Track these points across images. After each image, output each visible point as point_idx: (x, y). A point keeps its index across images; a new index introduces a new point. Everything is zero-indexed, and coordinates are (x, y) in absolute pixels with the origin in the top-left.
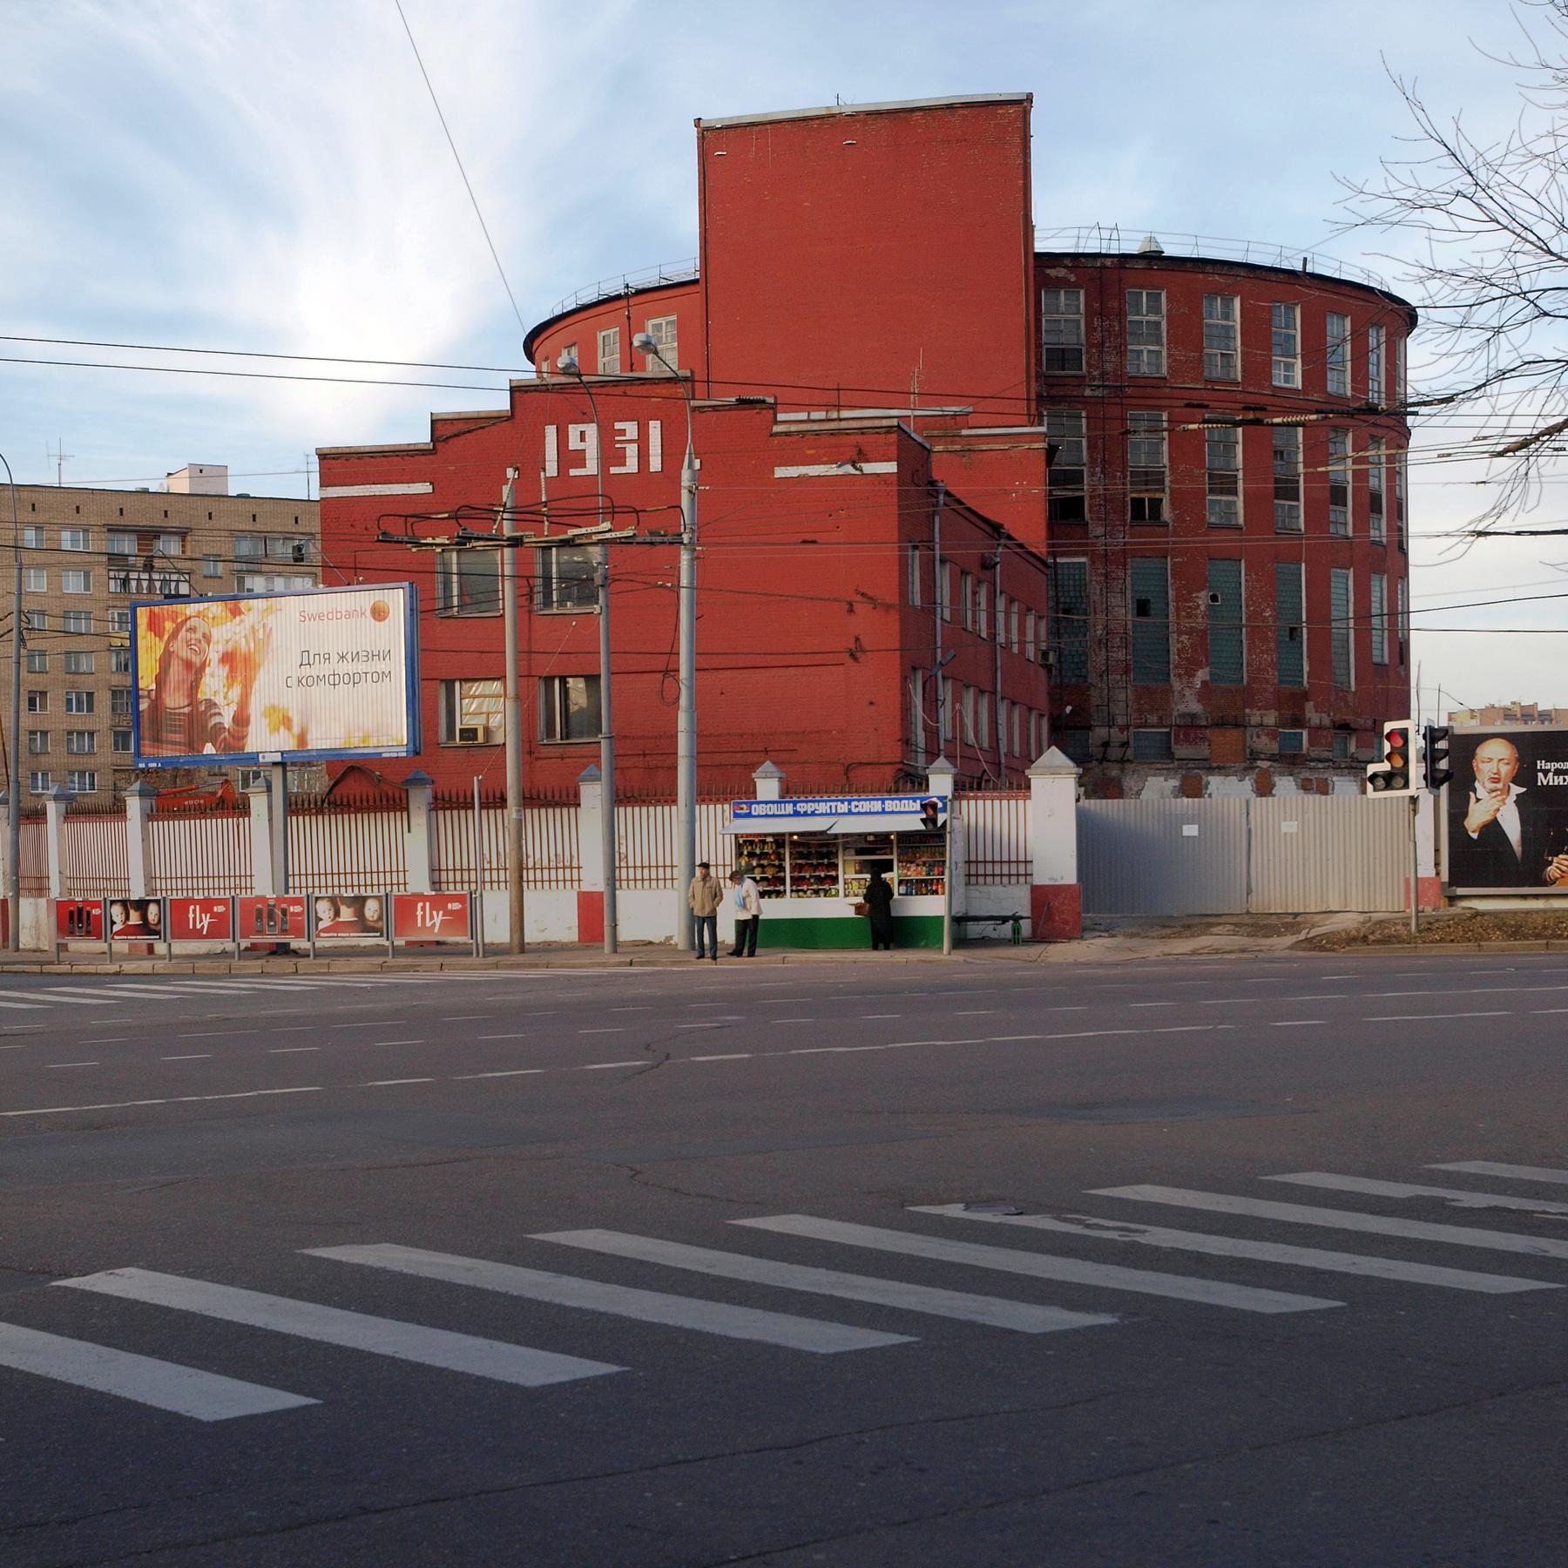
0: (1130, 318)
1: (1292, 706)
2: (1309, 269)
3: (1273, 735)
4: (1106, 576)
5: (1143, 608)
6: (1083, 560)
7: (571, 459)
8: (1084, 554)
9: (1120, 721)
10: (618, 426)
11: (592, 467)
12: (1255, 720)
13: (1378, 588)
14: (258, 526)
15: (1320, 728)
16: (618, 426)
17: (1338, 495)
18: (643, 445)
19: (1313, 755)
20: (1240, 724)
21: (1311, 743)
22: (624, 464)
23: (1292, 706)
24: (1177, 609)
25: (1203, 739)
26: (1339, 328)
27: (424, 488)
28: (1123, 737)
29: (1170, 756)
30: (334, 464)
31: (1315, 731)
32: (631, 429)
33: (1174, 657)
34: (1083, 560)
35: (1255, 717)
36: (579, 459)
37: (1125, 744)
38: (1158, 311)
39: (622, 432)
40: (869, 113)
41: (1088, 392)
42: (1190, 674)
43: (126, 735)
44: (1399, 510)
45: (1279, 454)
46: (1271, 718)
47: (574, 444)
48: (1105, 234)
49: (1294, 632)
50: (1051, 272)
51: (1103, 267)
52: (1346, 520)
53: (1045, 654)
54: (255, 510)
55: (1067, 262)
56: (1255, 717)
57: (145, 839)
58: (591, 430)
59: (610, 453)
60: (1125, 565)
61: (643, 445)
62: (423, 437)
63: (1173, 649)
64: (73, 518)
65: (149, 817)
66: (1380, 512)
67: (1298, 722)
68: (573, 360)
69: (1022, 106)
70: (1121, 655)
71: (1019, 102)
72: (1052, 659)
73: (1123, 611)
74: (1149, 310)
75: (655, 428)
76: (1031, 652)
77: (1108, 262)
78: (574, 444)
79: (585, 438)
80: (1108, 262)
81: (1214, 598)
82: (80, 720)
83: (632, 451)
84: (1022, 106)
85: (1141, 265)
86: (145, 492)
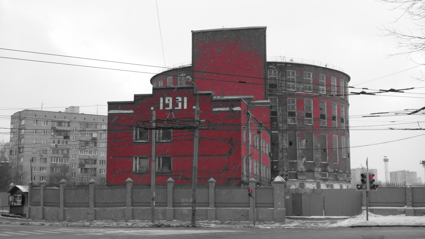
0: (288, 77)
1: (324, 167)
2: (327, 67)
3: (320, 174)
4: (283, 136)
5: (291, 144)
6: (277, 132)
7: (167, 105)
8: (277, 130)
9: (286, 170)
10: (177, 98)
11: (171, 107)
12: (316, 170)
13: (343, 139)
14: (86, 121)
15: (331, 172)
16: (177, 98)
17: (334, 118)
18: (183, 103)
19: (329, 179)
20: (313, 171)
21: (329, 176)
22: (169, 107)
23: (324, 167)
24: (299, 144)
25: (305, 175)
26: (334, 82)
27: (214, 110)
28: (286, 173)
29: (338, 180)
30: (112, 105)
31: (330, 173)
32: (180, 99)
33: (298, 155)
34: (277, 132)
35: (316, 169)
36: (168, 105)
37: (287, 175)
38: (294, 76)
39: (178, 99)
40: (230, 30)
41: (278, 94)
42: (301, 159)
43: (53, 168)
44: (347, 122)
45: (321, 109)
46: (320, 170)
47: (167, 102)
48: (282, 58)
49: (325, 150)
50: (270, 66)
51: (282, 66)
52: (336, 123)
53: (270, 154)
54: (85, 117)
55: (273, 64)
56: (316, 169)
57: (173, 193)
58: (171, 99)
59: (175, 104)
60: (287, 133)
61: (183, 103)
62: (132, 99)
63: (298, 153)
64: (45, 118)
65: (218, 185)
66: (343, 122)
67: (326, 171)
68: (166, 83)
69: (263, 30)
70: (286, 154)
71: (264, 28)
72: (272, 155)
73: (286, 144)
74: (292, 75)
75: (185, 99)
76: (267, 153)
77: (283, 64)
78: (167, 102)
79: (169, 100)
80: (283, 64)
81: (307, 142)
82: (43, 165)
83: (180, 104)
84: (263, 30)
85: (290, 65)
86: (60, 112)
